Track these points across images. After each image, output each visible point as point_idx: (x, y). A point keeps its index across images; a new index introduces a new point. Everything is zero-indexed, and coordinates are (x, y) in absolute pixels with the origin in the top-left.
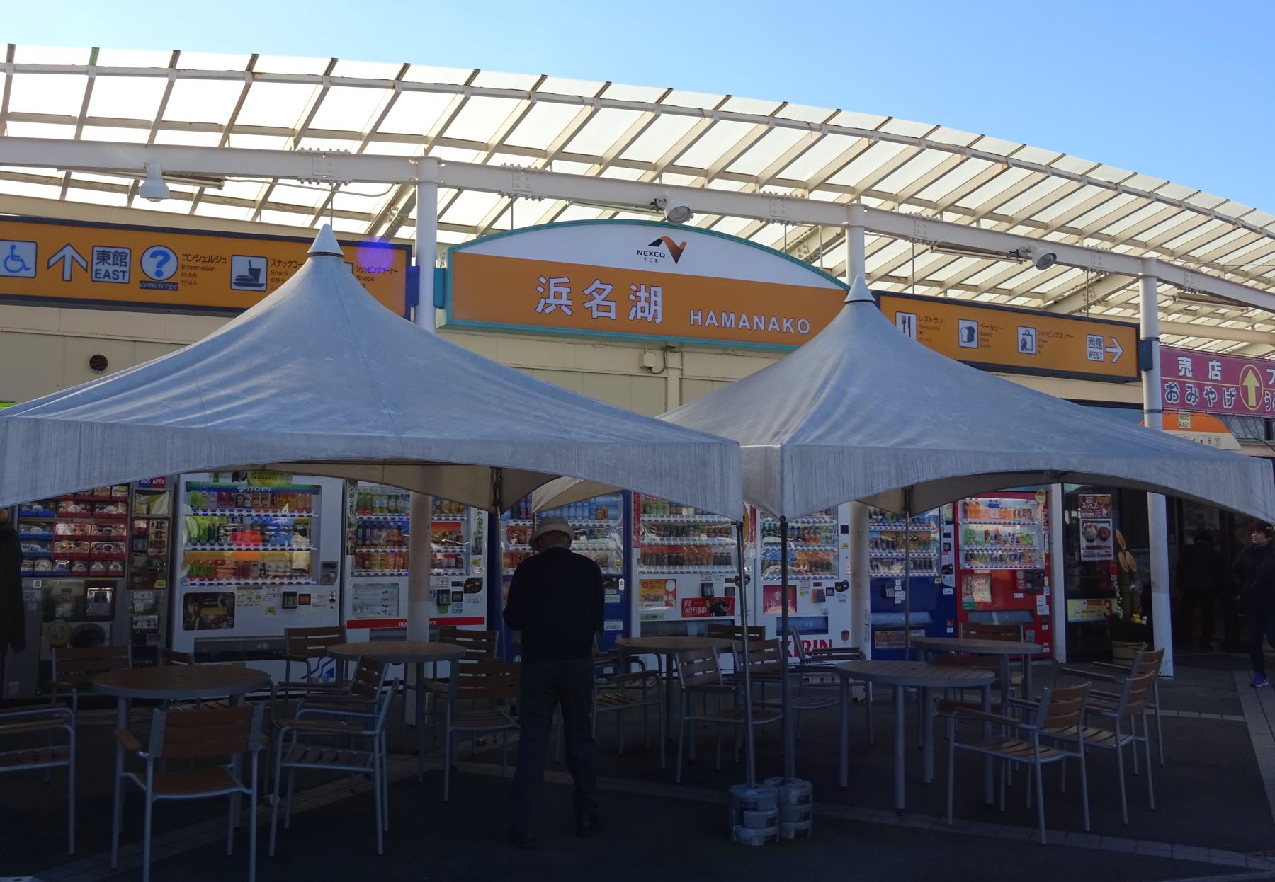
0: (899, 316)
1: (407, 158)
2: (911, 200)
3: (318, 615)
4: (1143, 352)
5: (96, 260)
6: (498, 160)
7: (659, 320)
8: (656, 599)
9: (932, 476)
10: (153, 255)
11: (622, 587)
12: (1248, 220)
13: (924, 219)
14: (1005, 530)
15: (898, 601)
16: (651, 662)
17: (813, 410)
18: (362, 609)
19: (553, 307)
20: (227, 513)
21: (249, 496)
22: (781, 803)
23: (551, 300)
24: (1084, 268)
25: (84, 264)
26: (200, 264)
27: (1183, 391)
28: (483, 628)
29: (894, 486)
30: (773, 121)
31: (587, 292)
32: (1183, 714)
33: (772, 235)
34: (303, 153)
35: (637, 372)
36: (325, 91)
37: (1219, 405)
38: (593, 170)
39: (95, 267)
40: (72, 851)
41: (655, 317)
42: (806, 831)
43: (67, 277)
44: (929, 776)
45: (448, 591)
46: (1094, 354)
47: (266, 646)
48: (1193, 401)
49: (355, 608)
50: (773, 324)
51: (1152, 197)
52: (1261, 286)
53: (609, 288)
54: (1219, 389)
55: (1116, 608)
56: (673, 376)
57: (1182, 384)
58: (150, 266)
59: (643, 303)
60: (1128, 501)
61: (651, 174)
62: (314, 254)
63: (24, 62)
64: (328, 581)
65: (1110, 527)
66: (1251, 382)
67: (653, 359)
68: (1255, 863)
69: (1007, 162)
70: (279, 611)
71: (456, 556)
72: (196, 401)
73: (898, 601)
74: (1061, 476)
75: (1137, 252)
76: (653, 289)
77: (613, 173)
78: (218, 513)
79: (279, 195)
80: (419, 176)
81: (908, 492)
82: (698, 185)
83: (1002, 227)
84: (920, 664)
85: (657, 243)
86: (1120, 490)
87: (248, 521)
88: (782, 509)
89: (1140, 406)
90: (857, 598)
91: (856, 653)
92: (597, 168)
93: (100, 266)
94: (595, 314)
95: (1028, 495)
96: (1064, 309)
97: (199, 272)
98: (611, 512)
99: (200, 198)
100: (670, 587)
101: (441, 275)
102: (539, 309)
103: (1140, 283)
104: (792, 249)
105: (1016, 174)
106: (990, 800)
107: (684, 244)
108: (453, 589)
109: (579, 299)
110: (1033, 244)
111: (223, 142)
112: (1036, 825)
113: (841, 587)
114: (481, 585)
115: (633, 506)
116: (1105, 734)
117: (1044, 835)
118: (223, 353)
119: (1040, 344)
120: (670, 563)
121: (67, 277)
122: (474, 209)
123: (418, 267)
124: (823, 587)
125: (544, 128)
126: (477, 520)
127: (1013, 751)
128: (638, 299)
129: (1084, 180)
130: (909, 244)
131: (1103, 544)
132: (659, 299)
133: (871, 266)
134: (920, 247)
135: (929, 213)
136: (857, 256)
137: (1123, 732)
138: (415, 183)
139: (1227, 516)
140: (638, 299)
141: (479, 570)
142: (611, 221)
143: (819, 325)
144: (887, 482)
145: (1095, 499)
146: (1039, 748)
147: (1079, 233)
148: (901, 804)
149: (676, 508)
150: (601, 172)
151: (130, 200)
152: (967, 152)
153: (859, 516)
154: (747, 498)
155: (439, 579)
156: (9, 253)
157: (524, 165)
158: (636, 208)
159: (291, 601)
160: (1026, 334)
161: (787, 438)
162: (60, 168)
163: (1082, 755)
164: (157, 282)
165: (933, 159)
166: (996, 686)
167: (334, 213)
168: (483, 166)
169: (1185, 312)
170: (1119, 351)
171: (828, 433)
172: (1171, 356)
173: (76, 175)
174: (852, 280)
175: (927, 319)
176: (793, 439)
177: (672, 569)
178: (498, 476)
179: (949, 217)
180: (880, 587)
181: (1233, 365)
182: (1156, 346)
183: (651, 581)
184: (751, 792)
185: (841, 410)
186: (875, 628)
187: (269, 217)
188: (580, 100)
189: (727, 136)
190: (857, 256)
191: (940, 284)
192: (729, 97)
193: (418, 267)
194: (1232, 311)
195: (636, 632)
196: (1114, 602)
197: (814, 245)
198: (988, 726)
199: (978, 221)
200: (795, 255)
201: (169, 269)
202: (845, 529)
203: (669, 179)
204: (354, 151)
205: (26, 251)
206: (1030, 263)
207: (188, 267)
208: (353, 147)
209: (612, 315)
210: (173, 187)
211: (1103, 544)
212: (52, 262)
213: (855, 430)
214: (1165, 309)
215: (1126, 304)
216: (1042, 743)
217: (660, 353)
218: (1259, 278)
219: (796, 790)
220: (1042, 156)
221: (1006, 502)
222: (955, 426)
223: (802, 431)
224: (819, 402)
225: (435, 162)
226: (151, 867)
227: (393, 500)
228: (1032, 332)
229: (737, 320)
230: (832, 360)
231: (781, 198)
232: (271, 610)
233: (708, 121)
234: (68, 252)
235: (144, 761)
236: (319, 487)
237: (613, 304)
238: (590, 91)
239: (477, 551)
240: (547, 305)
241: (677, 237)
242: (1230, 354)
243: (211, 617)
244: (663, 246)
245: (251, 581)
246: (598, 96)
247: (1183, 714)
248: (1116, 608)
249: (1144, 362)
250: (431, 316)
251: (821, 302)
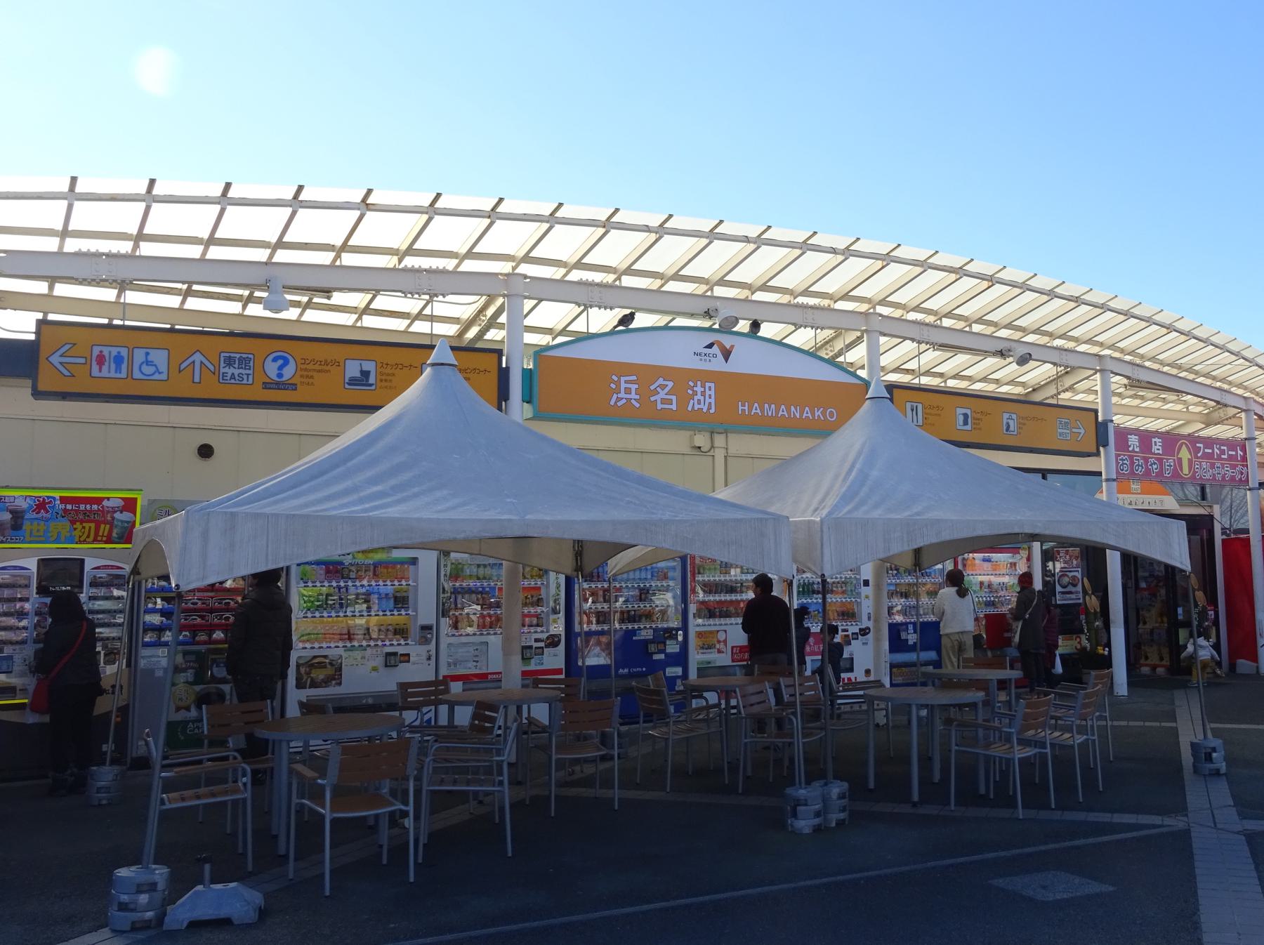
0: (909, 405)
1: (497, 274)
2: (917, 309)
3: (418, 670)
4: (1101, 431)
5: (222, 365)
6: (575, 275)
7: (712, 411)
8: (709, 647)
9: (934, 540)
10: (275, 360)
11: (680, 638)
12: (1178, 325)
13: (927, 325)
14: (996, 580)
15: (910, 643)
16: (712, 697)
17: (844, 489)
18: (455, 664)
19: (624, 401)
20: (334, 584)
21: (353, 568)
22: (825, 799)
23: (622, 395)
24: (1055, 364)
25: (212, 368)
26: (317, 367)
27: (1132, 463)
28: (563, 676)
29: (906, 548)
30: (805, 247)
31: (652, 388)
32: (1131, 723)
33: (803, 338)
34: (405, 270)
35: (688, 451)
36: (430, 220)
37: (1160, 474)
38: (654, 284)
39: (222, 370)
40: (250, 868)
41: (709, 408)
42: (844, 820)
43: (197, 379)
44: (937, 777)
45: (530, 647)
46: (1061, 435)
47: (370, 701)
48: (1140, 471)
49: (449, 664)
50: (807, 413)
51: (1104, 308)
52: (1191, 377)
53: (670, 384)
54: (1160, 460)
55: (1085, 643)
56: (719, 455)
57: (1131, 458)
58: (272, 369)
59: (699, 397)
60: (1093, 556)
61: (704, 288)
62: (433, 365)
63: (161, 193)
64: (424, 641)
65: (1079, 575)
66: (1185, 454)
67: (701, 440)
68: (1168, 821)
69: (992, 280)
70: (382, 670)
71: (537, 616)
72: (355, 497)
73: (910, 643)
74: (1034, 537)
75: (1095, 350)
76: (708, 385)
77: (673, 286)
78: (326, 584)
79: (382, 302)
80: (511, 289)
81: (918, 552)
82: (742, 297)
83: (989, 330)
84: (929, 689)
85: (710, 346)
86: (1087, 547)
87: (352, 590)
88: (822, 569)
89: (1100, 474)
90: (878, 640)
91: (878, 684)
92: (658, 282)
93: (226, 370)
94: (660, 406)
95: (1015, 551)
96: (1038, 397)
97: (315, 374)
98: (670, 574)
99: (309, 305)
100: (722, 636)
101: (528, 375)
102: (612, 403)
103: (1098, 375)
104: (818, 349)
105: (999, 290)
106: (982, 791)
107: (732, 347)
108: (536, 645)
109: (646, 393)
110: (1014, 345)
111: (335, 260)
112: (1016, 807)
113: (864, 632)
114: (559, 641)
115: (688, 567)
116: (1067, 735)
117: (1020, 813)
118: (369, 452)
119: (1021, 426)
120: (720, 617)
121: (197, 379)
122: (551, 315)
123: (507, 368)
124: (850, 633)
125: (616, 250)
126: (555, 583)
127: (998, 750)
128: (695, 393)
129: (1052, 294)
130: (915, 345)
131: (1073, 589)
132: (712, 393)
133: (885, 360)
134: (923, 347)
135: (930, 319)
136: (874, 353)
137: (1079, 733)
138: (504, 296)
139: (1167, 566)
140: (695, 393)
141: (558, 628)
142: (666, 328)
143: (846, 415)
144: (901, 547)
145: (1067, 552)
146: (1017, 748)
147: (1050, 334)
148: (916, 797)
149: (726, 567)
150: (662, 286)
151: (244, 307)
152: (960, 272)
153: (878, 574)
154: (795, 560)
155: (532, 637)
156: (144, 359)
157: (597, 280)
158: (692, 316)
159: (392, 660)
160: (1010, 418)
161: (825, 512)
162: (183, 283)
163: (1048, 750)
164: (277, 383)
165: (933, 277)
166: (986, 703)
167: (432, 318)
168: (562, 281)
169: (1135, 396)
170: (1082, 431)
171: (856, 508)
172: (1123, 434)
173: (195, 287)
174: (870, 373)
175: (931, 407)
176: (830, 513)
177: (723, 621)
178: (579, 548)
179: (947, 322)
180: (895, 630)
181: (1171, 440)
182: (1111, 426)
183: (705, 632)
184: (802, 792)
185: (865, 489)
186: (892, 666)
187: (369, 321)
188: (647, 229)
189: (767, 259)
190: (874, 353)
191: (941, 375)
192: (769, 227)
193: (507, 368)
194: (1172, 397)
195: (693, 675)
196: (1083, 637)
197: (839, 345)
198: (981, 732)
199: (970, 326)
200: (823, 354)
201: (289, 372)
202: (866, 583)
203: (719, 291)
204: (450, 268)
205: (160, 357)
206: (1011, 359)
207: (306, 370)
208: (450, 264)
209: (674, 407)
210: (289, 297)
211: (1073, 589)
212: (183, 366)
213: (876, 506)
214: (1120, 395)
215: (1090, 391)
216: (1019, 744)
217: (708, 435)
218: (1189, 370)
219: (836, 789)
220: (1019, 275)
221: (995, 556)
222: (950, 500)
223: (836, 507)
224: (848, 484)
225: (521, 278)
226: (331, 871)
227: (481, 569)
228: (1014, 416)
229: (777, 411)
230: (857, 446)
231: (811, 307)
232: (375, 669)
233: (753, 246)
234: (198, 358)
235: (323, 787)
236: (416, 559)
237: (674, 398)
238: (655, 222)
239: (555, 611)
240: (619, 399)
241: (727, 341)
242: (1168, 432)
243: (321, 677)
244: (715, 349)
245: (356, 644)
246: (661, 225)
247: (1131, 723)
248: (1085, 643)
249: (1102, 440)
250: (518, 409)
251: (847, 395)
